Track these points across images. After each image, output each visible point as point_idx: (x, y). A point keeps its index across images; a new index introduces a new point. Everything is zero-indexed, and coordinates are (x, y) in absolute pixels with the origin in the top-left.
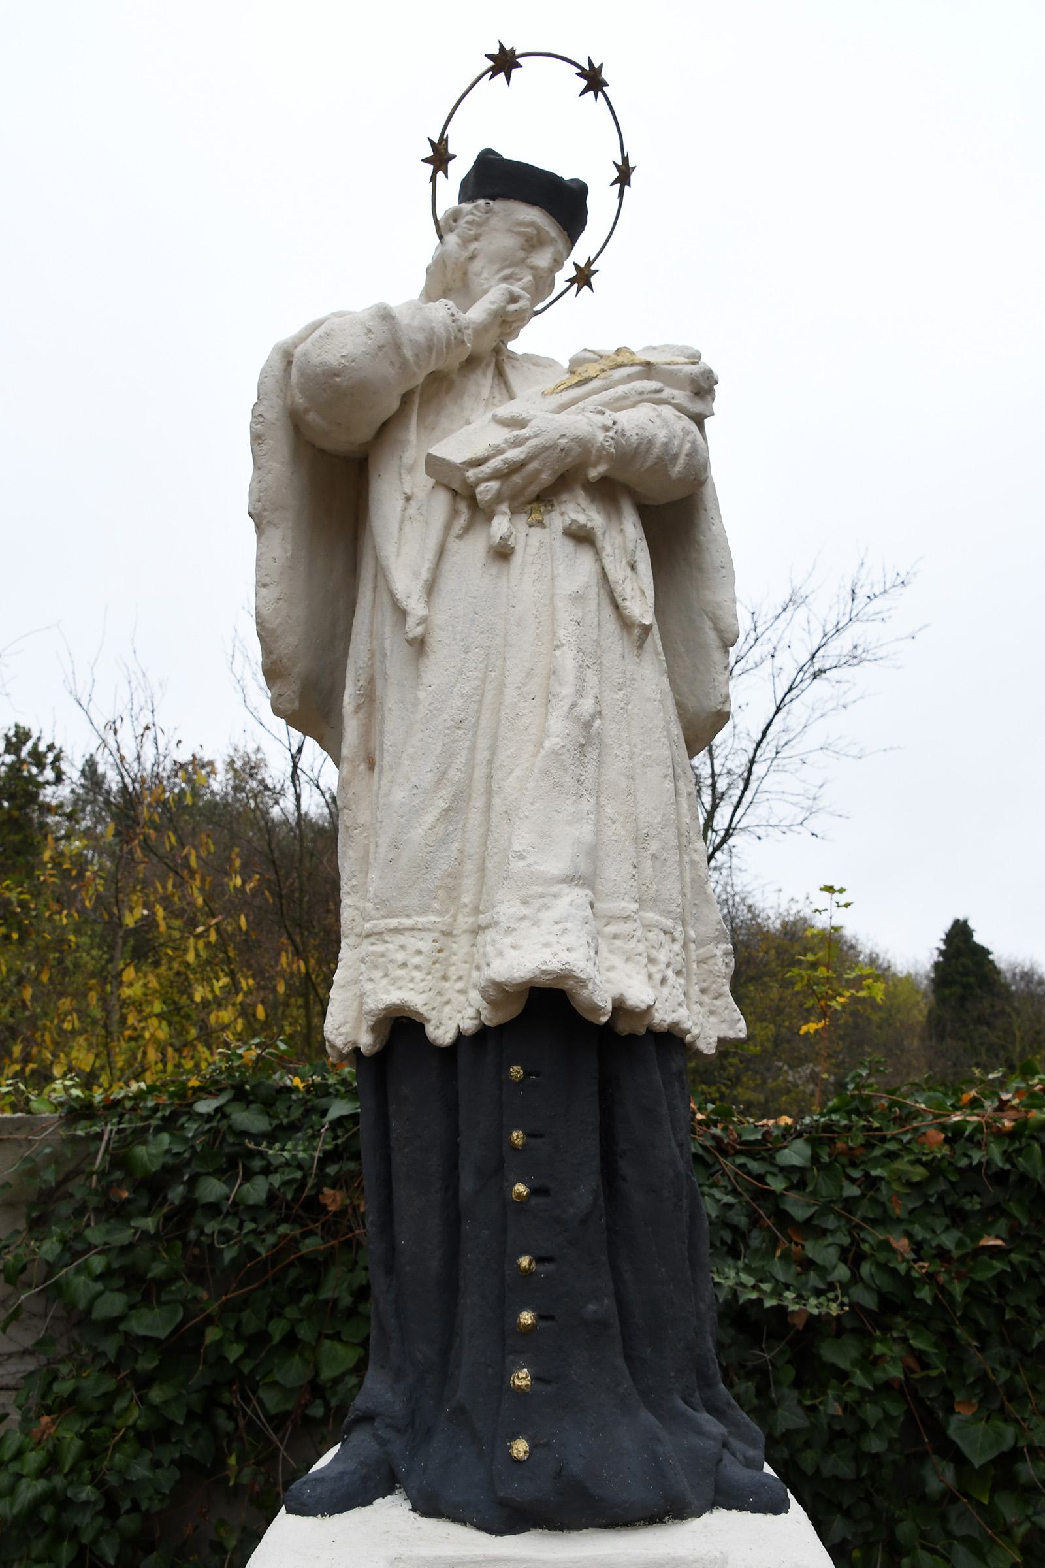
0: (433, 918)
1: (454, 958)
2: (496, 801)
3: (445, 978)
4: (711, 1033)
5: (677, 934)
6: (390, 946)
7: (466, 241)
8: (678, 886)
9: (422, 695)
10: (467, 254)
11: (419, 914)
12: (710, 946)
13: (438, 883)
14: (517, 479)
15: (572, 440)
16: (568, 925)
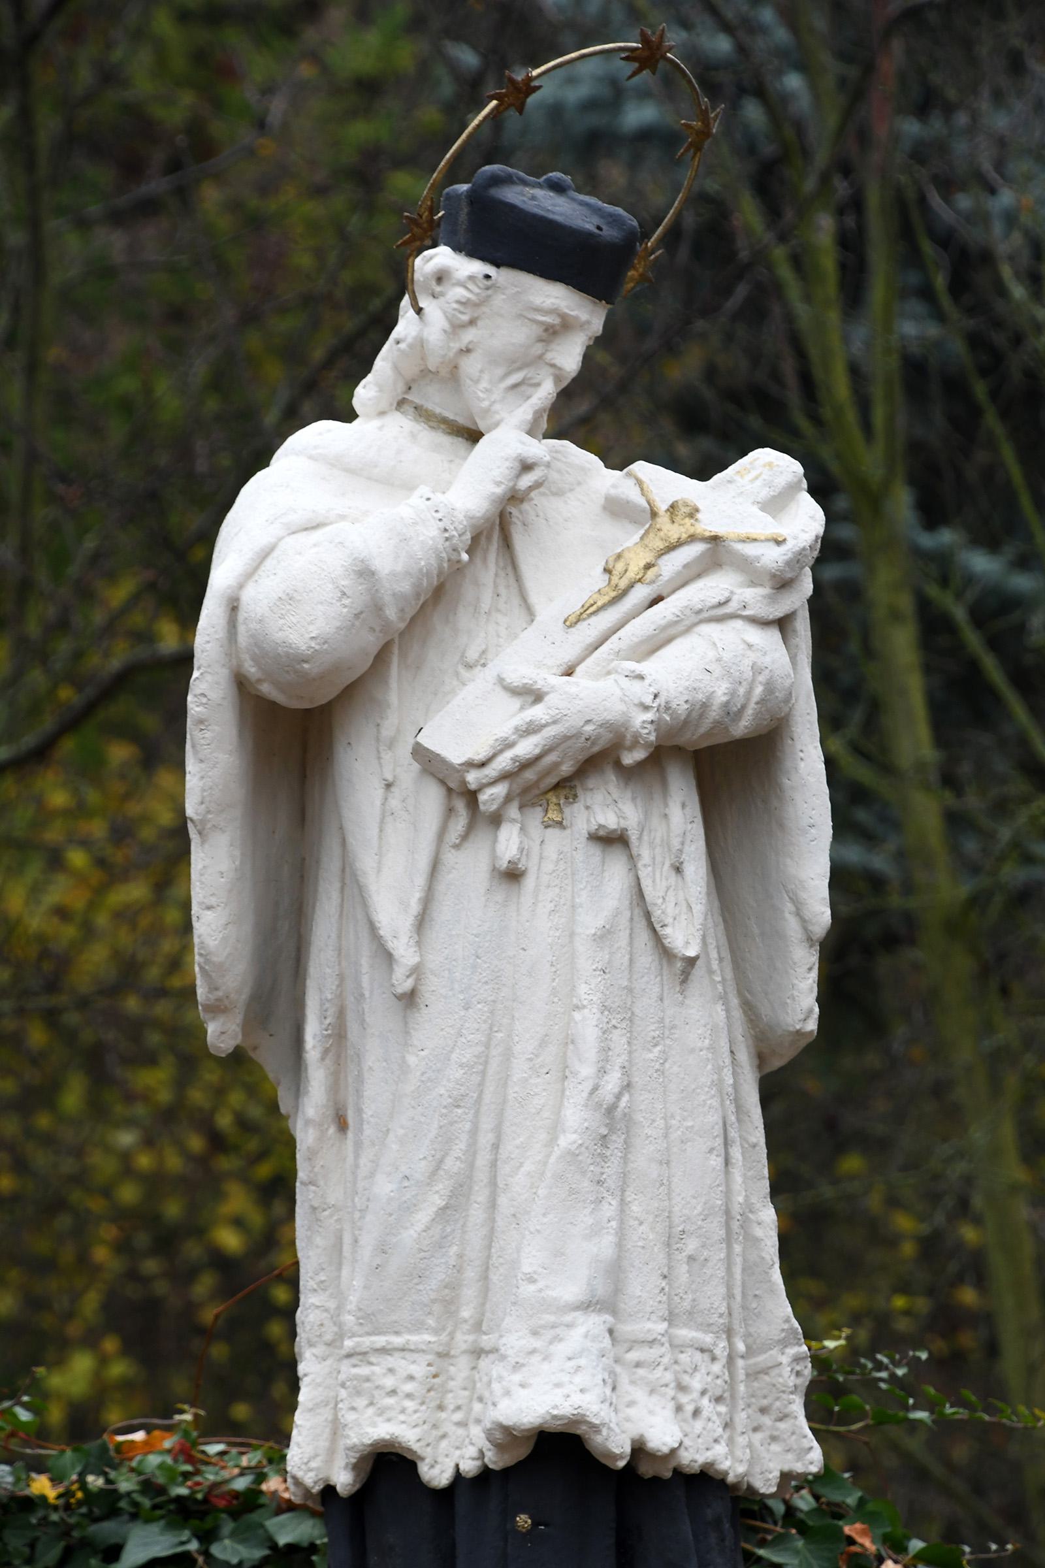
0: (427, 1337)
1: (452, 1384)
2: (502, 1200)
3: (441, 1408)
4: (771, 1465)
5: (718, 1352)
6: (376, 1369)
7: (456, 327)
8: (722, 1290)
9: (412, 1060)
10: (455, 346)
11: (410, 1331)
12: (774, 1352)
13: (433, 1296)
14: (530, 775)
15: (601, 726)
16: (582, 1362)
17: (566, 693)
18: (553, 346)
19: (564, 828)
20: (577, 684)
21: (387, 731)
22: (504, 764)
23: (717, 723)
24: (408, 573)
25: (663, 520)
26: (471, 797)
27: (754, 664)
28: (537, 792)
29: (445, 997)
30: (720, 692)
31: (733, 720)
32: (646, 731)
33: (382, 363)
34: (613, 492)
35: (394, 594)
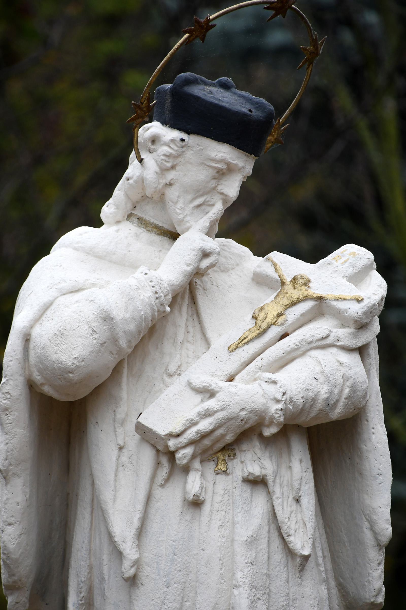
7: (163, 170)
10: (163, 182)
14: (207, 442)
15: (250, 412)
17: (229, 392)
18: (222, 182)
19: (228, 475)
20: (236, 386)
22: (191, 435)
23: (321, 411)
24: (133, 319)
25: (289, 287)
26: (171, 455)
28: (211, 452)
29: (154, 580)
30: (323, 392)
31: (331, 409)
34: (258, 270)
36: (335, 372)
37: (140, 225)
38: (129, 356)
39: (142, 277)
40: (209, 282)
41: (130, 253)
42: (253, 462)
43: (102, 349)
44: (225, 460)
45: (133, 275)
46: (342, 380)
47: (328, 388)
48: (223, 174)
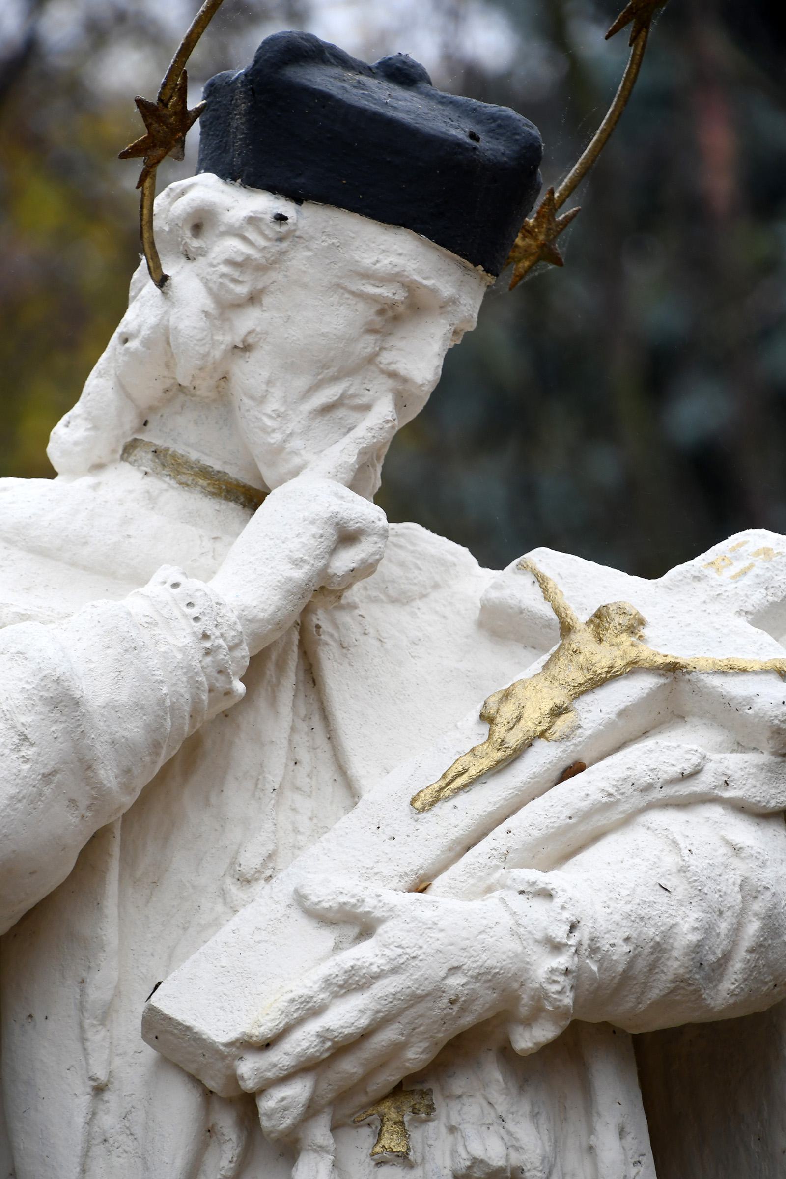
7: (226, 307)
10: (226, 339)
14: (350, 1066)
15: (477, 978)
17: (414, 919)
18: (393, 341)
19: (411, 1166)
20: (434, 905)
21: (97, 994)
22: (305, 1044)
23: (681, 982)
24: (138, 706)
25: (583, 638)
26: (246, 1104)
27: (745, 880)
28: (363, 1099)
30: (685, 927)
31: (709, 979)
32: (557, 988)
33: (99, 384)
34: (494, 595)
35: (113, 743)
36: (718, 871)
37: (159, 468)
38: (126, 818)
39: (166, 594)
40: (356, 629)
41: (132, 540)
42: (484, 1128)
43: (47, 791)
44: (402, 1123)
45: (140, 590)
46: (739, 897)
47: (701, 915)
48: (397, 319)
